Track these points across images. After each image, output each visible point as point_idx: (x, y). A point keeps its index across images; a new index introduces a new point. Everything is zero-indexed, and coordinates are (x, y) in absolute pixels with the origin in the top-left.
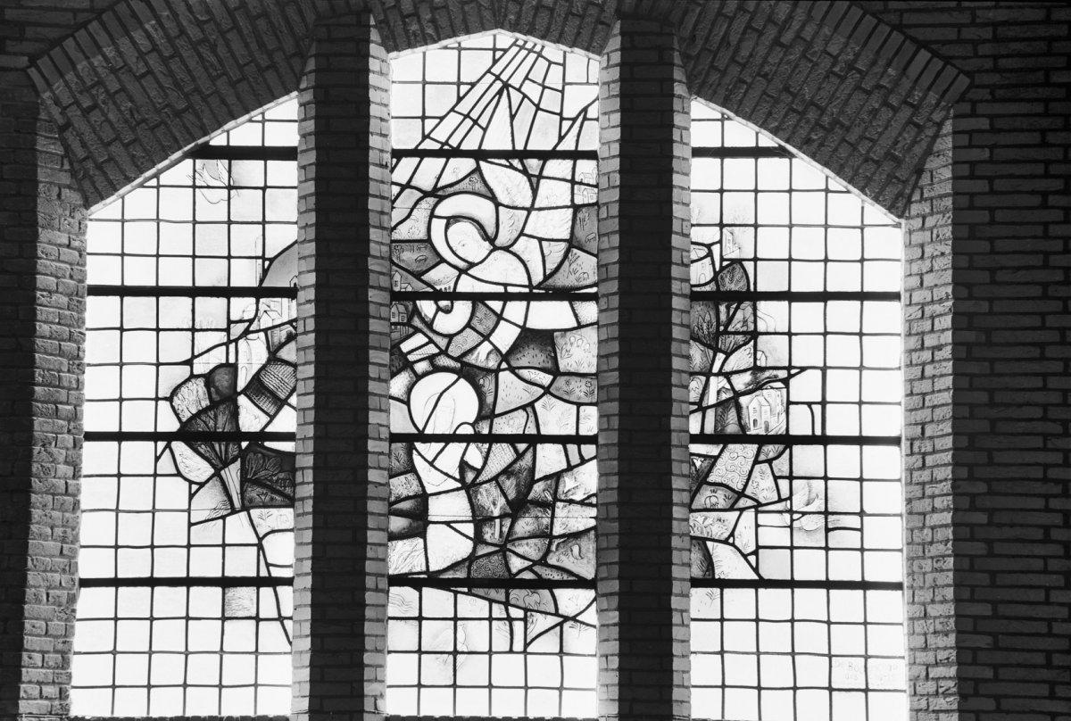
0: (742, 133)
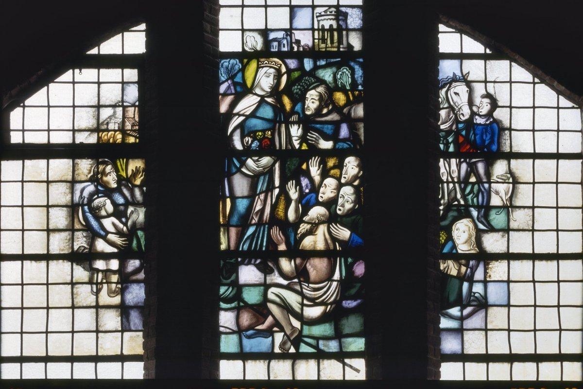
0: (473, 46)
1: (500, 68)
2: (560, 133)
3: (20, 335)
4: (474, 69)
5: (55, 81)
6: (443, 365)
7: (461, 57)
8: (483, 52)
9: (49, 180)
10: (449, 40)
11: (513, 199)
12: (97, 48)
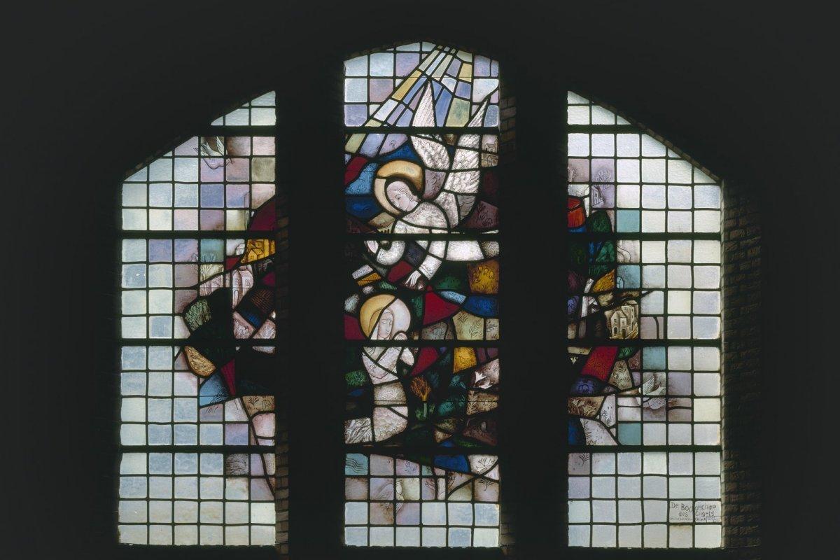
0: (603, 117)
1: (629, 143)
2: (664, 207)
3: (170, 527)
4: (603, 144)
5: (166, 155)
6: (124, 454)
7: (591, 129)
8: (613, 123)
9: (669, 338)
10: (577, 114)
11: (650, 287)
12: (221, 118)
